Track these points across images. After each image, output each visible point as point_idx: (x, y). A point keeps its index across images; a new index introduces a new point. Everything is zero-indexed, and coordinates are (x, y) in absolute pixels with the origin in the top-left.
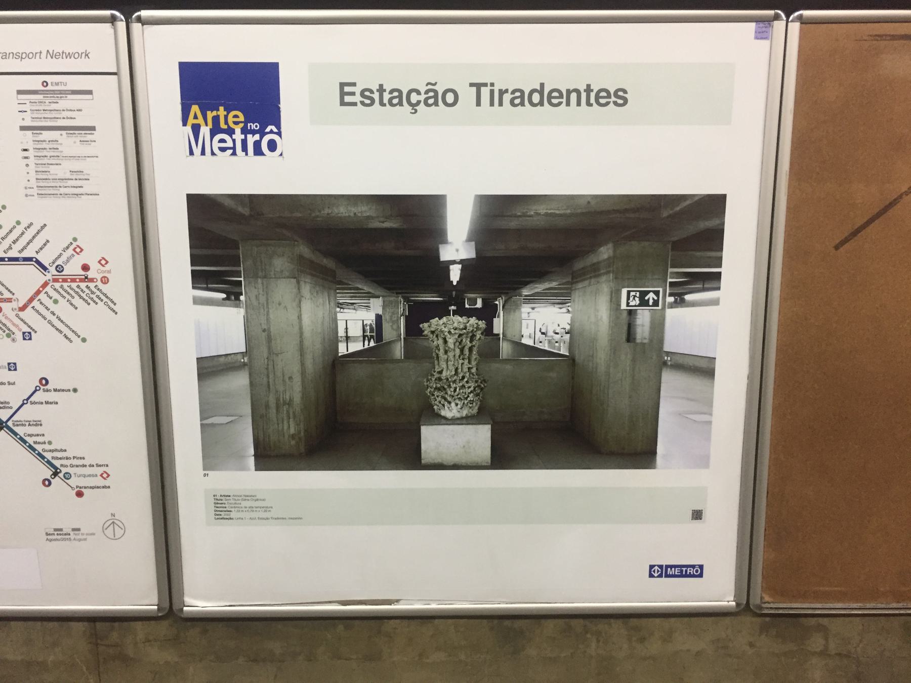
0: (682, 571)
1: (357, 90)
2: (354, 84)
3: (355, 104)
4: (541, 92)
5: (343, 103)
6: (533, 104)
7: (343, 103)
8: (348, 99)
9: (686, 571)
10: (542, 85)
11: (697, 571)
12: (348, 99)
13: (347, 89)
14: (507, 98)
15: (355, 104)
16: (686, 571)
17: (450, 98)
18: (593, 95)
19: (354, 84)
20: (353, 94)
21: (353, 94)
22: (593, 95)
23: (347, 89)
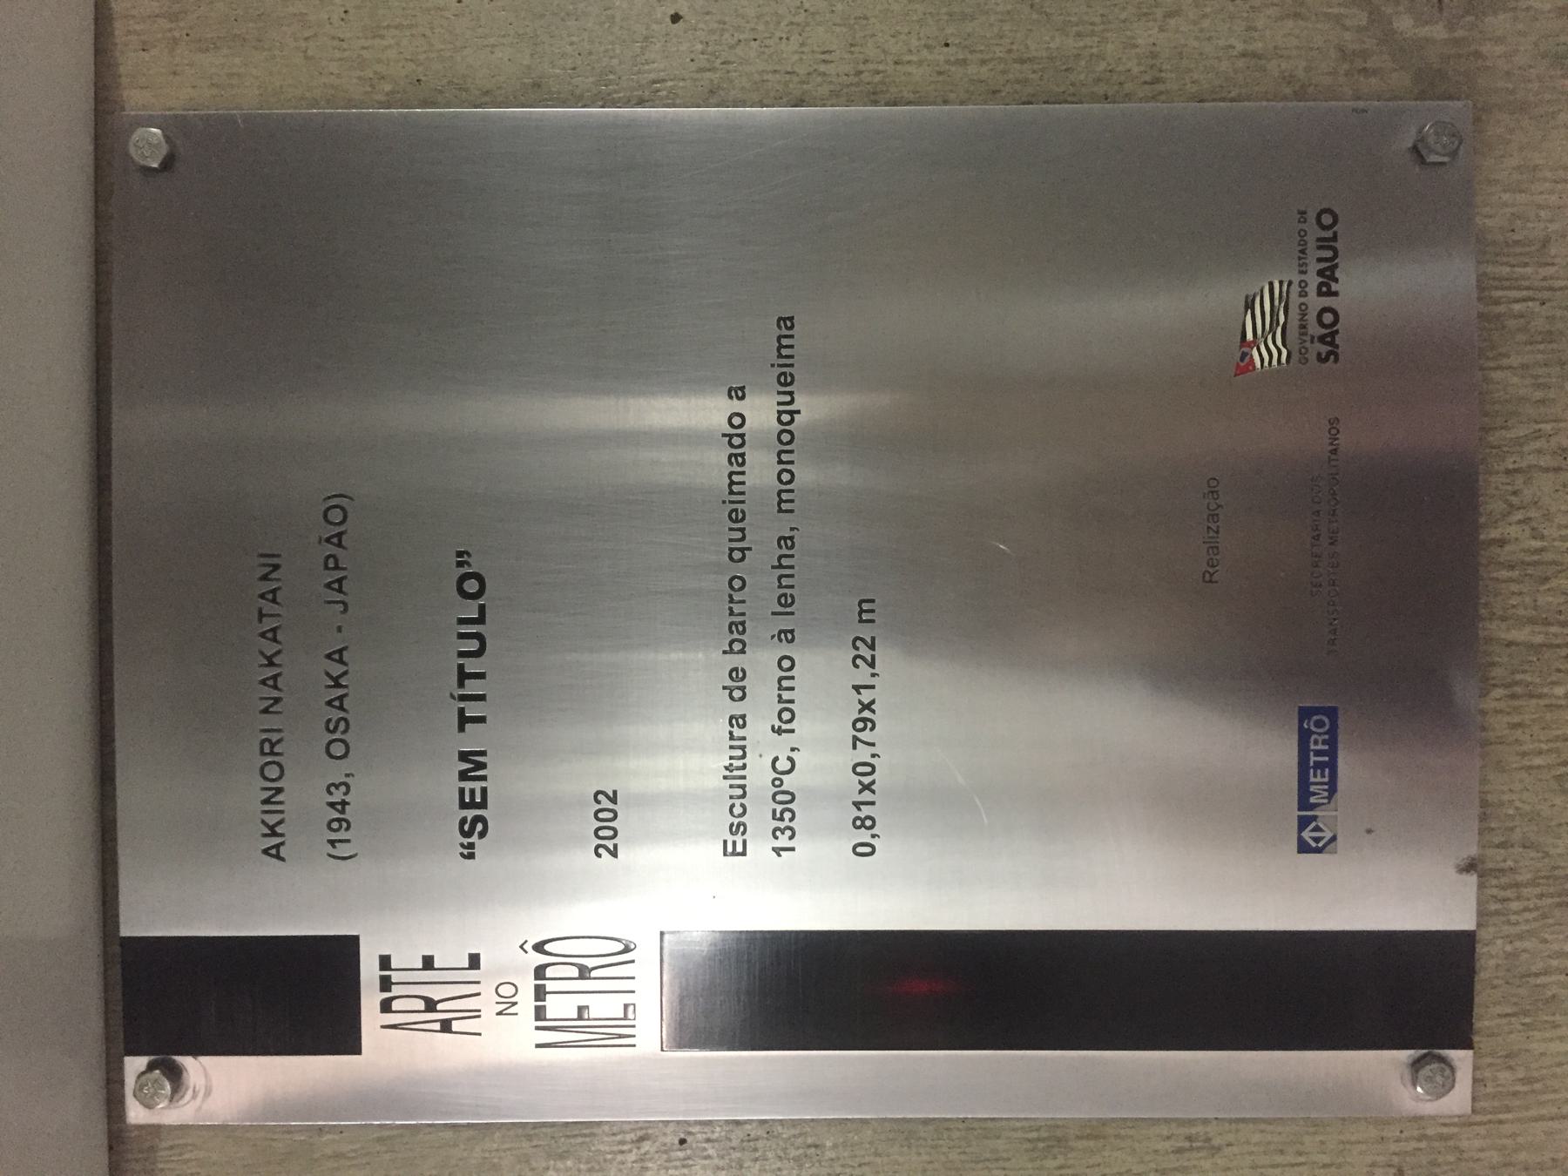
0: (1318, 765)
1: (730, 839)
2: (725, 842)
3: (744, 842)
4: (731, 436)
5: (744, 854)
6: (780, 680)
7: (744, 854)
8: (739, 849)
9: (1318, 753)
10: (724, 435)
11: (1319, 724)
12: (739, 849)
13: (730, 849)
14: (786, 695)
15: (744, 842)
16: (1318, 753)
17: (338, 749)
18: (784, 727)
19: (725, 842)
20: (734, 843)
21: (734, 843)
22: (784, 727)
23: (730, 849)
